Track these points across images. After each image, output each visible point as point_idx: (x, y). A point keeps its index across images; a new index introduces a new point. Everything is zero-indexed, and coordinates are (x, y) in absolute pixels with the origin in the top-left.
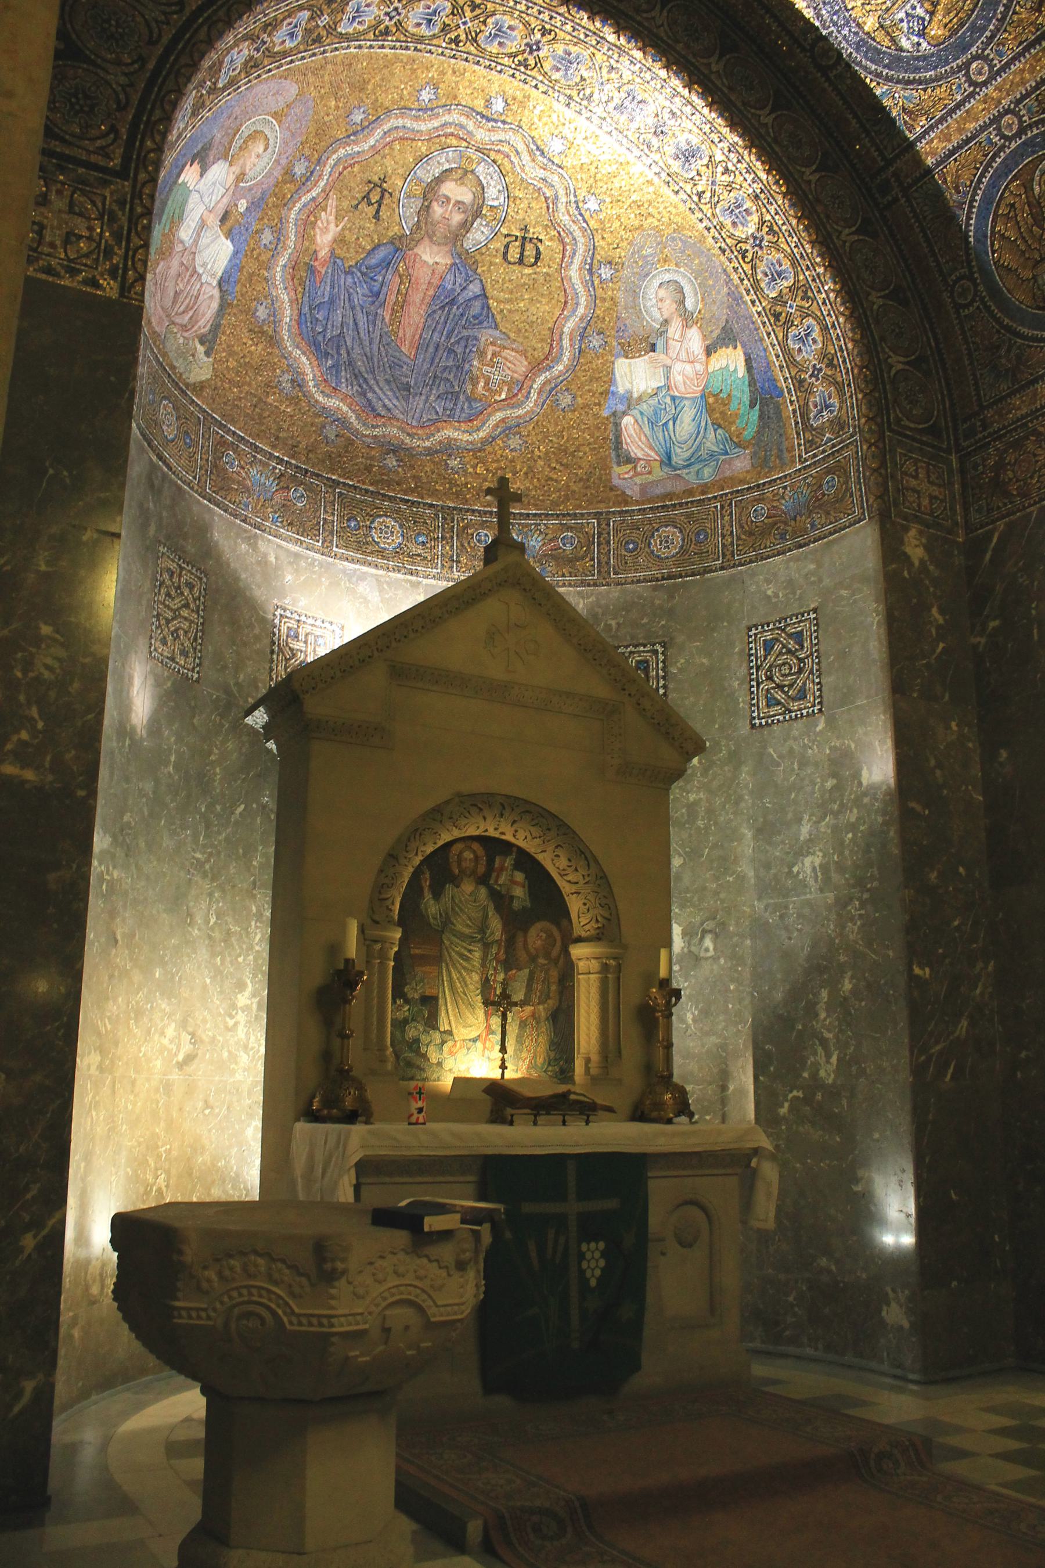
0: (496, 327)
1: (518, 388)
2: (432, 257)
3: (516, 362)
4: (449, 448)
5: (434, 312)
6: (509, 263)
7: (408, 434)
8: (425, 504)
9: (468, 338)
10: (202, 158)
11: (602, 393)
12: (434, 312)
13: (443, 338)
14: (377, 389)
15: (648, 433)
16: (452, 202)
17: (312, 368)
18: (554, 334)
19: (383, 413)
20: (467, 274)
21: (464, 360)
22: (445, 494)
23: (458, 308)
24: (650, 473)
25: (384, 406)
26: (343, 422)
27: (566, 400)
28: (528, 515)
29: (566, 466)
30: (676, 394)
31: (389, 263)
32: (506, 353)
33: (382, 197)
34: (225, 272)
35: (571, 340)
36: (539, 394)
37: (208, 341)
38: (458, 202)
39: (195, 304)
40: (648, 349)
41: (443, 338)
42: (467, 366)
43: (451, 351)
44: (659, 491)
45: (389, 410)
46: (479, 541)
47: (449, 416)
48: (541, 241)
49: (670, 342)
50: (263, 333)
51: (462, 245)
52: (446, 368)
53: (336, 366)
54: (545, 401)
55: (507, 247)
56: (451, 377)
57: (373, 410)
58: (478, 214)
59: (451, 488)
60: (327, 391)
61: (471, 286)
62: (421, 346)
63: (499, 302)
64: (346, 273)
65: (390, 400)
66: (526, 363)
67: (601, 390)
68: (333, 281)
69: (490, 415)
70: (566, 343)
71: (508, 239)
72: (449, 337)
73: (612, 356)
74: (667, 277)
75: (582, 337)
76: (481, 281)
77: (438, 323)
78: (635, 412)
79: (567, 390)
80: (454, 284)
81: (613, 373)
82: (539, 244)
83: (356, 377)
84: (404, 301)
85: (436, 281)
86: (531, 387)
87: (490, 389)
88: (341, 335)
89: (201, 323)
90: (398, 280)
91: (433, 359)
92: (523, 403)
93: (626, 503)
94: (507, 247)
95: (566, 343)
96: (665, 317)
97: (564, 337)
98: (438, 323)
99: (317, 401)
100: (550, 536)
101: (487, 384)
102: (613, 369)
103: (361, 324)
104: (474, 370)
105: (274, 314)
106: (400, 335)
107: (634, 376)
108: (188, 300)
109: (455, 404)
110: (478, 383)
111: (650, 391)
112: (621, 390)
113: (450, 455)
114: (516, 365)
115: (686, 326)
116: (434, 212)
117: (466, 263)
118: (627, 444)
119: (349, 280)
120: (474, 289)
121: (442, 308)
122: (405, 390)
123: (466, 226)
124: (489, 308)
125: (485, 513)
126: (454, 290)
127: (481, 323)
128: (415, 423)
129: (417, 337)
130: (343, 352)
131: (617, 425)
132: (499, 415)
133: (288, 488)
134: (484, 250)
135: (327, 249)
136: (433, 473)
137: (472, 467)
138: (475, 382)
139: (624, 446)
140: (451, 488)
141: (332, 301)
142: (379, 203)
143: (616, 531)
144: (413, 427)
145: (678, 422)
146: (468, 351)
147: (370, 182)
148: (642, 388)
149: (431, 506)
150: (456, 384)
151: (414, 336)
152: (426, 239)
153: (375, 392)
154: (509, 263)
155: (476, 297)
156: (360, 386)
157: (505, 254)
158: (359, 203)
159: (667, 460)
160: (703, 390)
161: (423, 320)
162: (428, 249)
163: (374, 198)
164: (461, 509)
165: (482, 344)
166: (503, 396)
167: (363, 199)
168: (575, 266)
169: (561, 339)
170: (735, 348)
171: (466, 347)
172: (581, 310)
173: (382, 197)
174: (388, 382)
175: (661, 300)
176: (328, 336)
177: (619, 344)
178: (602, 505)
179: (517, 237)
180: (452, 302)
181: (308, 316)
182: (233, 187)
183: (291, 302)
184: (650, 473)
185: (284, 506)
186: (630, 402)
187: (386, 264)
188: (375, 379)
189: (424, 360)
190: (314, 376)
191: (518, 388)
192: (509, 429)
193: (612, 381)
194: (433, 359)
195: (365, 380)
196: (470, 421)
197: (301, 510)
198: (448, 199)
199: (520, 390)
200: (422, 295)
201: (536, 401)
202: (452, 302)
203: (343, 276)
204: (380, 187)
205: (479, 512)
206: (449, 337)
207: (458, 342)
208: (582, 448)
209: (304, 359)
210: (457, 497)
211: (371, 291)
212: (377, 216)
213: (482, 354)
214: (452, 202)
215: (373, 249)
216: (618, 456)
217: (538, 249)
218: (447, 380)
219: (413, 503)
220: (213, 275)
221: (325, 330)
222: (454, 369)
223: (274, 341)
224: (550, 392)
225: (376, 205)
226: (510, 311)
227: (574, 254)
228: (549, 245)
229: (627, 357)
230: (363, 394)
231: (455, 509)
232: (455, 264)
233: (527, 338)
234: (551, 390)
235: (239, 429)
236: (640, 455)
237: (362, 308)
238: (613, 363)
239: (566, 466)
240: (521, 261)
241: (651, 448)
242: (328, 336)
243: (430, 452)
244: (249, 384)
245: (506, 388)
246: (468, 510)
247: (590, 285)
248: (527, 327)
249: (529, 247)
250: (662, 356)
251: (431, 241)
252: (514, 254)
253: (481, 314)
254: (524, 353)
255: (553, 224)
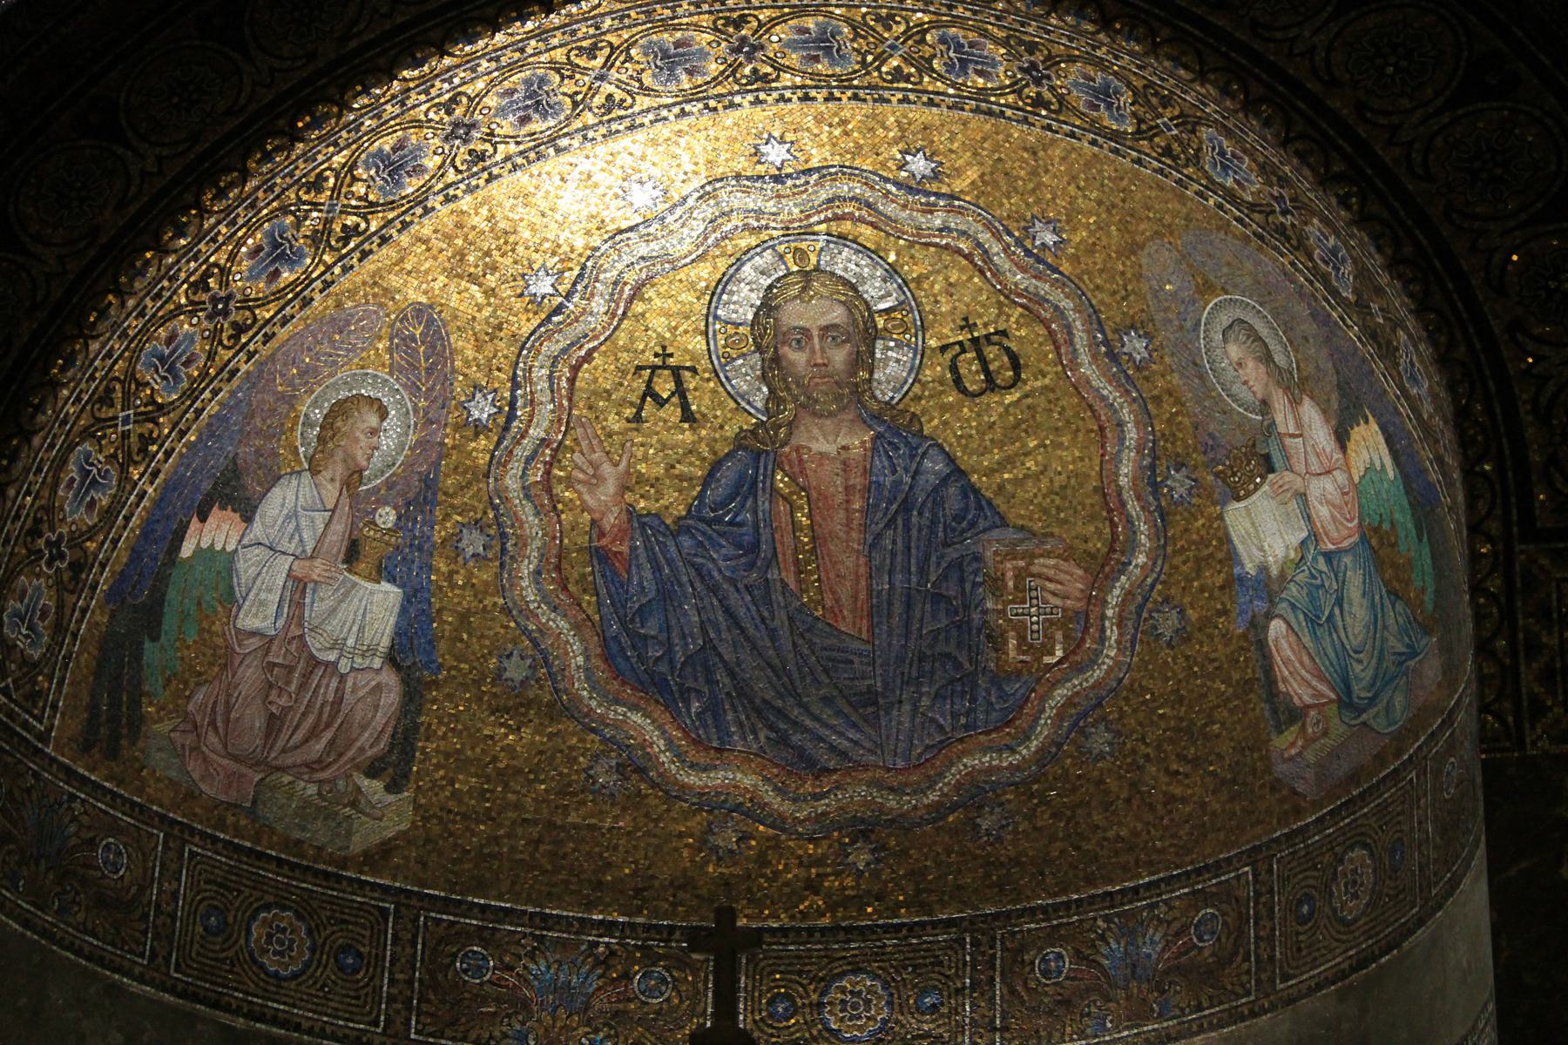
0: (1004, 523)
1: (1080, 624)
2: (832, 442)
3: (1062, 576)
4: (975, 794)
5: (878, 536)
6: (974, 395)
7: (892, 789)
8: (934, 925)
9: (958, 565)
10: (235, 493)
11: (1222, 588)
12: (878, 536)
13: (914, 579)
14: (808, 722)
15: (1310, 645)
16: (815, 333)
17: (659, 728)
18: (1108, 501)
19: (832, 765)
20: (907, 444)
21: (966, 607)
22: (976, 891)
23: (920, 514)
24: (1325, 733)
25: (832, 748)
26: (753, 811)
27: (1168, 623)
28: (1136, 890)
29: (1195, 762)
30: (1331, 547)
31: (754, 483)
32: (1040, 565)
33: (679, 382)
34: (399, 633)
35: (1138, 498)
36: (1119, 626)
37: (394, 765)
38: (825, 329)
39: (332, 717)
40: (1262, 470)
41: (914, 579)
42: (976, 616)
43: (937, 598)
44: (1341, 769)
45: (843, 754)
46: (1046, 973)
47: (966, 727)
48: (1004, 333)
49: (1288, 441)
50: (529, 704)
51: (874, 397)
52: (935, 634)
53: (713, 709)
54: (1134, 637)
55: (954, 368)
56: (951, 648)
57: (811, 763)
58: (870, 335)
59: (988, 875)
60: (703, 759)
61: (928, 464)
62: (876, 611)
63: (989, 472)
64: (675, 535)
65: (841, 734)
66: (1080, 572)
67: (1219, 580)
68: (653, 560)
69: (1043, 699)
70: (1133, 507)
71: (949, 355)
72: (923, 572)
73: (1215, 503)
74: (1225, 319)
75: (1155, 487)
76: (940, 447)
77: (893, 554)
78: (1283, 607)
79: (1167, 600)
80: (894, 472)
81: (1229, 541)
82: (1006, 343)
83: (759, 712)
84: (813, 539)
85: (857, 480)
86: (1103, 617)
87: (1031, 646)
88: (709, 646)
89: (365, 738)
90: (782, 507)
91: (907, 626)
92: (1098, 653)
93: (1298, 812)
94: (954, 368)
95: (1133, 507)
96: (1259, 396)
97: (1125, 496)
98: (893, 554)
99: (684, 786)
100: (1176, 926)
101: (1021, 638)
102: (1226, 528)
103: (742, 612)
104: (990, 617)
105: (544, 659)
106: (829, 603)
107: (1263, 531)
108: (311, 719)
109: (973, 700)
110: (1006, 643)
111: (1292, 555)
112: (1250, 568)
113: (981, 807)
114: (1065, 583)
115: (1295, 402)
116: (792, 364)
117: (896, 429)
118: (1284, 680)
119: (686, 542)
120: (934, 466)
121: (891, 523)
122: (869, 705)
123: (863, 360)
124: (976, 491)
125: (1056, 908)
126: (897, 484)
127: (972, 525)
128: (900, 764)
129: (862, 596)
130: (721, 676)
131: (1262, 644)
132: (1060, 694)
133: (627, 976)
134: (917, 389)
135: (616, 510)
136: (949, 852)
137: (1025, 817)
138: (997, 641)
139: (1282, 687)
140: (988, 875)
141: (667, 595)
142: (680, 391)
143: (1284, 880)
144: (899, 771)
145: (1346, 606)
146: (968, 586)
147: (639, 368)
148: (1280, 552)
149: (950, 923)
150: (963, 658)
151: (855, 597)
152: (802, 413)
153: (806, 730)
154: (974, 395)
155: (945, 481)
156: (771, 728)
157: (958, 381)
158: (640, 409)
159: (1347, 703)
160: (1360, 524)
161: (862, 560)
162: (816, 431)
163: (665, 387)
164: (1008, 915)
165: (990, 563)
166: (1059, 653)
167: (643, 400)
168: (1084, 357)
169: (1123, 504)
170: (1367, 422)
171: (962, 580)
172: (1132, 434)
173: (679, 382)
174: (827, 701)
175: (1240, 364)
176: (680, 657)
177: (1217, 475)
178: (1259, 829)
179: (960, 343)
180: (906, 507)
181: (624, 639)
182: (345, 500)
183: (577, 627)
184: (1325, 733)
185: (616, 1014)
186: (1267, 586)
187: (746, 488)
188: (800, 705)
189: (890, 634)
190: (670, 743)
191: (1080, 624)
192: (1081, 715)
193: (1232, 557)
194: (907, 626)
195: (781, 713)
196: (1008, 724)
197: (658, 1013)
198: (805, 331)
199: (1085, 630)
200: (842, 515)
201: (1118, 642)
202: (906, 507)
203: (670, 543)
204: (664, 367)
205: (1044, 909)
206: (923, 572)
207: (944, 577)
208: (1217, 716)
209: (636, 718)
210: (1001, 890)
211: (739, 546)
212: (687, 416)
213: (996, 585)
214: (815, 333)
215: (711, 474)
216: (1275, 711)
217: (1008, 350)
218: (948, 655)
219: (911, 927)
220: (371, 651)
221: (670, 650)
222: (954, 632)
223: (562, 709)
224: (1139, 615)
225: (675, 400)
226: (1017, 482)
227: (1070, 333)
228: (1022, 333)
229: (1238, 499)
230: (783, 741)
231: (995, 916)
232: (879, 436)
233: (1066, 521)
234: (1138, 610)
235: (500, 898)
236: (1308, 699)
237: (732, 581)
238: (1221, 517)
239: (1195, 762)
240: (991, 385)
241: (1321, 678)
242: (680, 657)
243: (939, 811)
244: (517, 806)
245: (1059, 636)
246: (1022, 913)
247: (1125, 383)
248: (1058, 501)
249: (991, 352)
250: (1288, 476)
251: (814, 414)
252: (974, 382)
253: (966, 509)
254: (1068, 554)
255: (1007, 295)
